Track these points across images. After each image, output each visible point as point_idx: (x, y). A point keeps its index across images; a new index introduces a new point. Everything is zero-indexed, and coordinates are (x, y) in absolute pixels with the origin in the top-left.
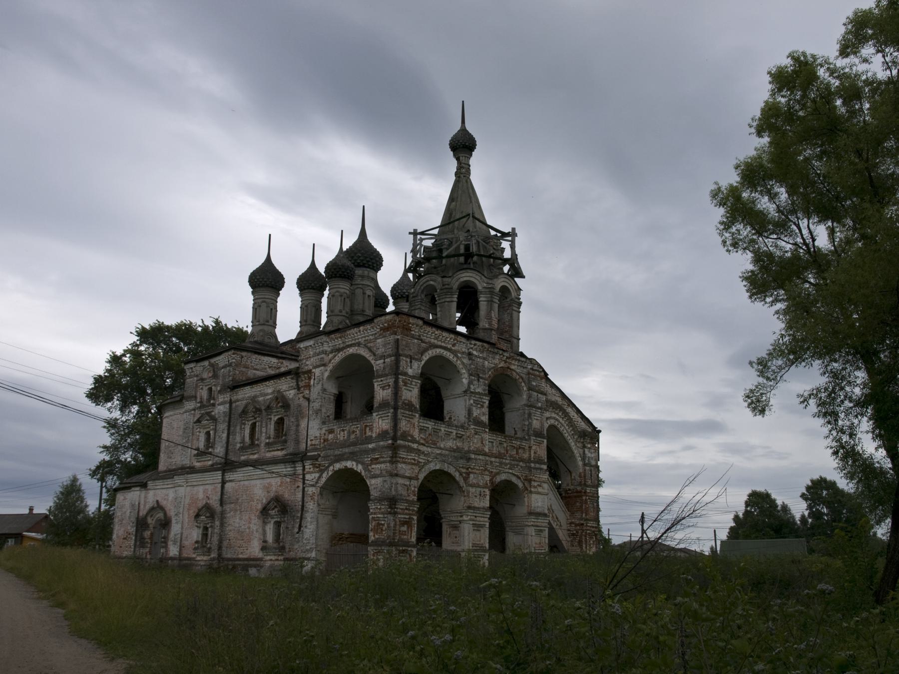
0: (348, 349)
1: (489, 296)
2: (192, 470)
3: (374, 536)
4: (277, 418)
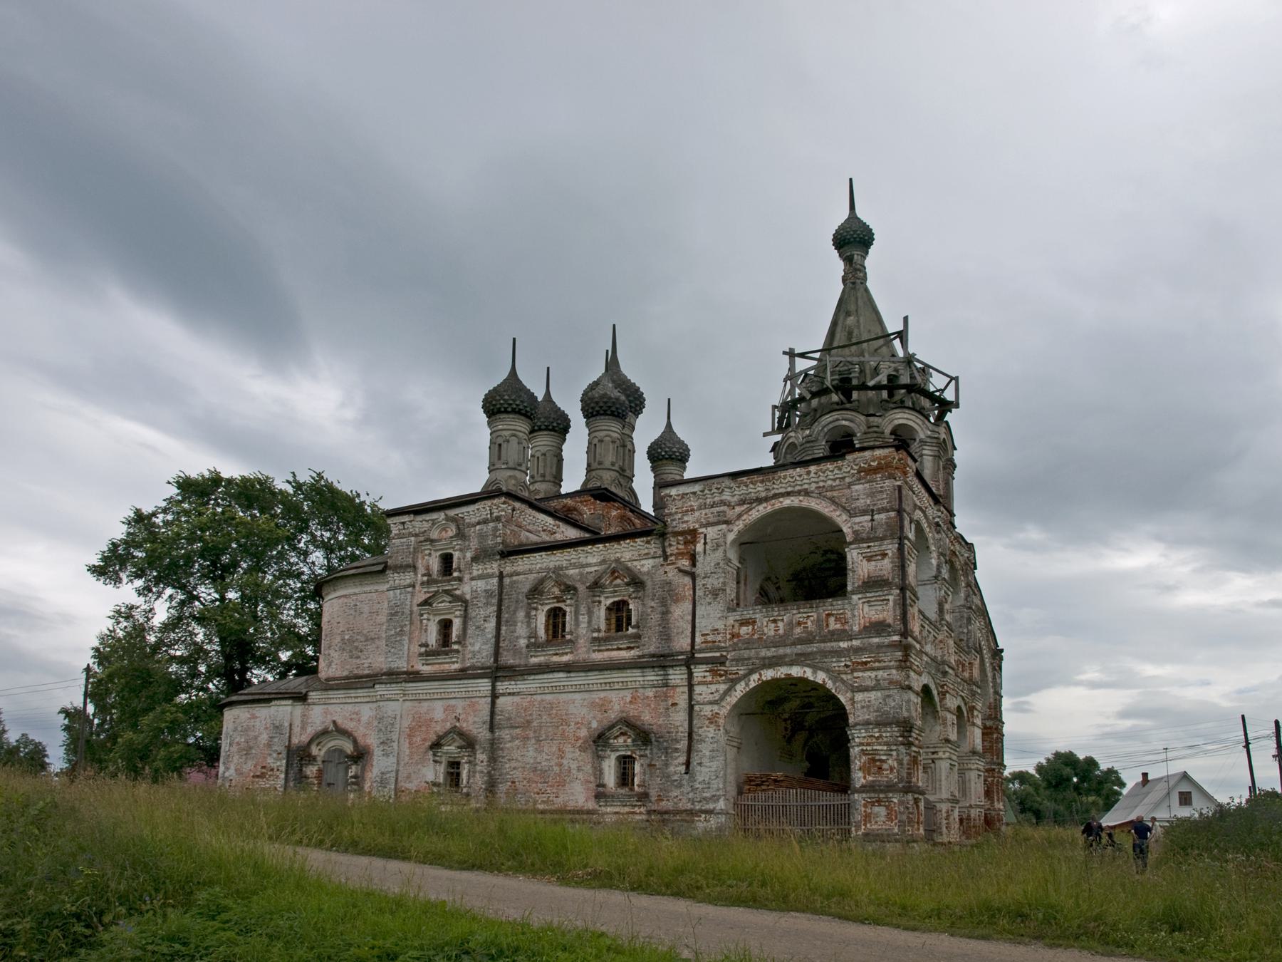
0: (781, 499)
1: (935, 448)
2: (414, 677)
4: (611, 601)
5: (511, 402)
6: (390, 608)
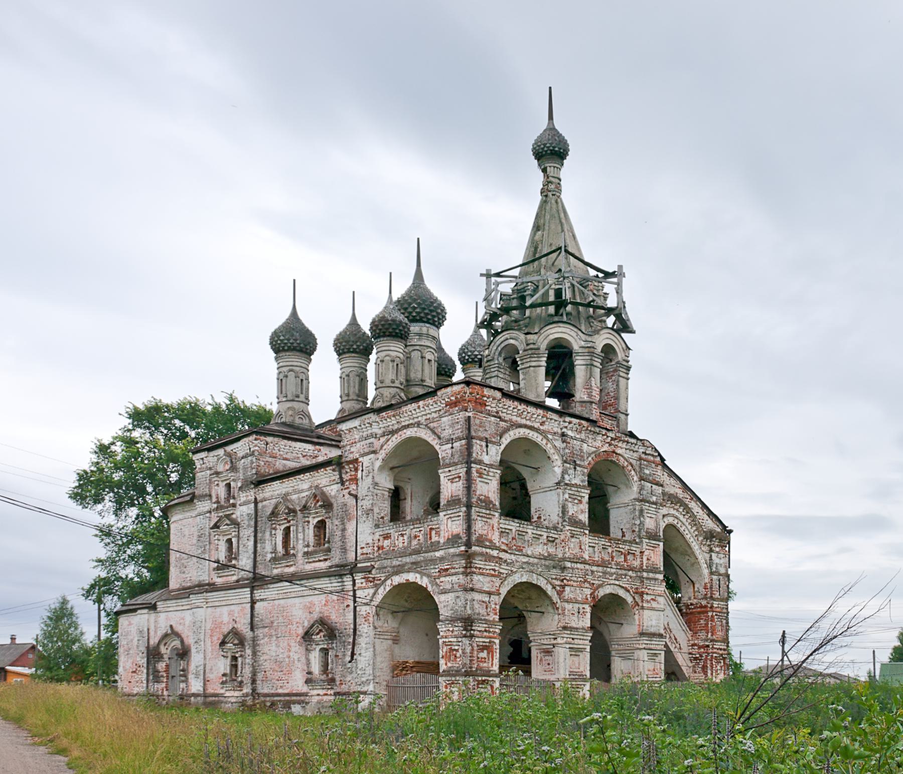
1: (587, 358)
2: (212, 587)
3: (446, 664)
4: (316, 520)
5: (286, 341)
6: (199, 531)
